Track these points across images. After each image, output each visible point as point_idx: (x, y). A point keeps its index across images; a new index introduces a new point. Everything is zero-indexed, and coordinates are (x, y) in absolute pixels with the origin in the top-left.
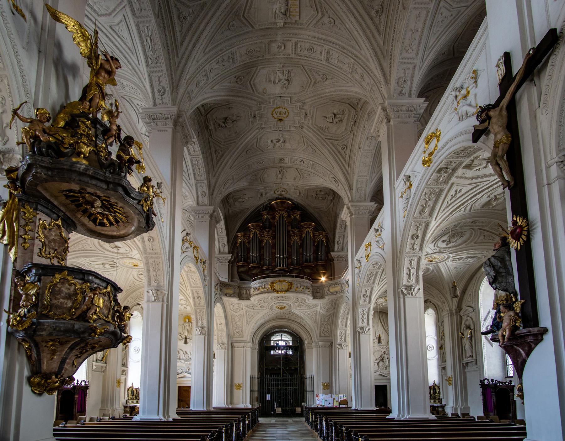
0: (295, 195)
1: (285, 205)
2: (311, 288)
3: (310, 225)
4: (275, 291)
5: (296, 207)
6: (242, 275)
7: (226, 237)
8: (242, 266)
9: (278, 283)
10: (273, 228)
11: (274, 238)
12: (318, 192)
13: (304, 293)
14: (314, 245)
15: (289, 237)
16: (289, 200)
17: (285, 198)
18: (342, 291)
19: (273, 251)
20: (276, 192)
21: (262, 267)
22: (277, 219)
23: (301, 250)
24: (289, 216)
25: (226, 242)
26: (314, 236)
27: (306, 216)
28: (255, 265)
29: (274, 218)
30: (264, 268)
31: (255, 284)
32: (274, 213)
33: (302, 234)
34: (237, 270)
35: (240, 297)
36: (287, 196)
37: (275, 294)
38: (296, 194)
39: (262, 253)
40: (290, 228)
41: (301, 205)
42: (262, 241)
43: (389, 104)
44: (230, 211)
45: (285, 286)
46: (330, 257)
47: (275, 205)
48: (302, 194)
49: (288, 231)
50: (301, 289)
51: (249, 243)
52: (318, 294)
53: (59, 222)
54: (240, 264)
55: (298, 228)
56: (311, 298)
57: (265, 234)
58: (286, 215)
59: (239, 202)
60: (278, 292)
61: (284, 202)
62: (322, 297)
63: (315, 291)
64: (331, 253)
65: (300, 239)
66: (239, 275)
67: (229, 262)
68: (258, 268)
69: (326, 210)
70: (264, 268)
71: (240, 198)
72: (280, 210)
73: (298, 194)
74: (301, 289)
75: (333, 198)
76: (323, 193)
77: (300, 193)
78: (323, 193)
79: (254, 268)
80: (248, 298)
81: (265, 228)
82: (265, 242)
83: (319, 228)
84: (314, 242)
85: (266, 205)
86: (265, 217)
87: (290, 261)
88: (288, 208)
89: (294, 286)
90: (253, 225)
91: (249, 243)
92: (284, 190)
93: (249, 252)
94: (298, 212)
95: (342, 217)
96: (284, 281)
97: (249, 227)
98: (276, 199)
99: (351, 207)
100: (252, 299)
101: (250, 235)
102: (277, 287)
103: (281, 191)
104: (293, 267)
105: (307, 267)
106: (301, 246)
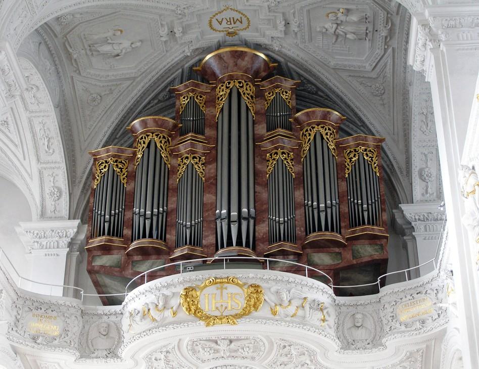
0: (270, 33)
1: (244, 63)
2: (331, 310)
3: (325, 116)
4: (197, 313)
5: (276, 69)
6: (106, 280)
7: (63, 166)
8: (106, 249)
9: (212, 289)
10: (208, 132)
11: (211, 158)
12: (342, 17)
13: (303, 322)
14: (340, 177)
15: (259, 153)
16: (258, 47)
17: (246, 44)
18: (441, 313)
19: (208, 198)
20: (215, 24)
21: (171, 250)
22: (223, 102)
23: (298, 195)
24: (259, 94)
25: (62, 182)
26: (340, 147)
27: (311, 93)
28: (145, 242)
29: (212, 101)
30: (178, 253)
31: (138, 298)
32: (214, 89)
33: (300, 145)
34: (89, 263)
35: (86, 350)
36: (248, 35)
37: (200, 330)
38: (275, 27)
39: (172, 205)
40: (261, 129)
41: (294, 61)
42: (173, 171)
43: (430, 15)
44: (79, 87)
45: (235, 298)
46: (399, 221)
47: (216, 67)
48: (294, 27)
49: (257, 139)
50: (292, 309)
51: (131, 176)
52: (360, 334)
53: (61, 349)
54: (97, 241)
55: (289, 127)
56: (333, 344)
57: (183, 149)
58: (248, 90)
59: (106, 56)
60: (208, 319)
61: (241, 55)
62: (375, 342)
63: (348, 324)
64: (403, 207)
65: (297, 159)
66: (96, 284)
67: (71, 245)
68: (158, 252)
69: (373, 75)
70: (178, 253)
71: (106, 41)
72: (231, 78)
73: (281, 27)
74: (292, 309)
75: (391, 32)
76: (354, 18)
77: (287, 24)
78: (354, 18)
79: (144, 252)
80: (112, 353)
81: (183, 132)
82: (182, 170)
83: (352, 123)
84: (341, 167)
85: (191, 68)
86: (184, 101)
87: (263, 229)
88: (256, 74)
89: (268, 296)
90: (144, 123)
91: (131, 176)
92: (237, 16)
93: (130, 205)
94: (288, 84)
95: (410, 61)
96: (232, 281)
97: (133, 131)
98: (219, 47)
99: (430, 20)
100: (125, 351)
101: (135, 154)
102: (208, 301)
103: (229, 21)
104: (275, 247)
105: (318, 246)
106: (300, 180)
